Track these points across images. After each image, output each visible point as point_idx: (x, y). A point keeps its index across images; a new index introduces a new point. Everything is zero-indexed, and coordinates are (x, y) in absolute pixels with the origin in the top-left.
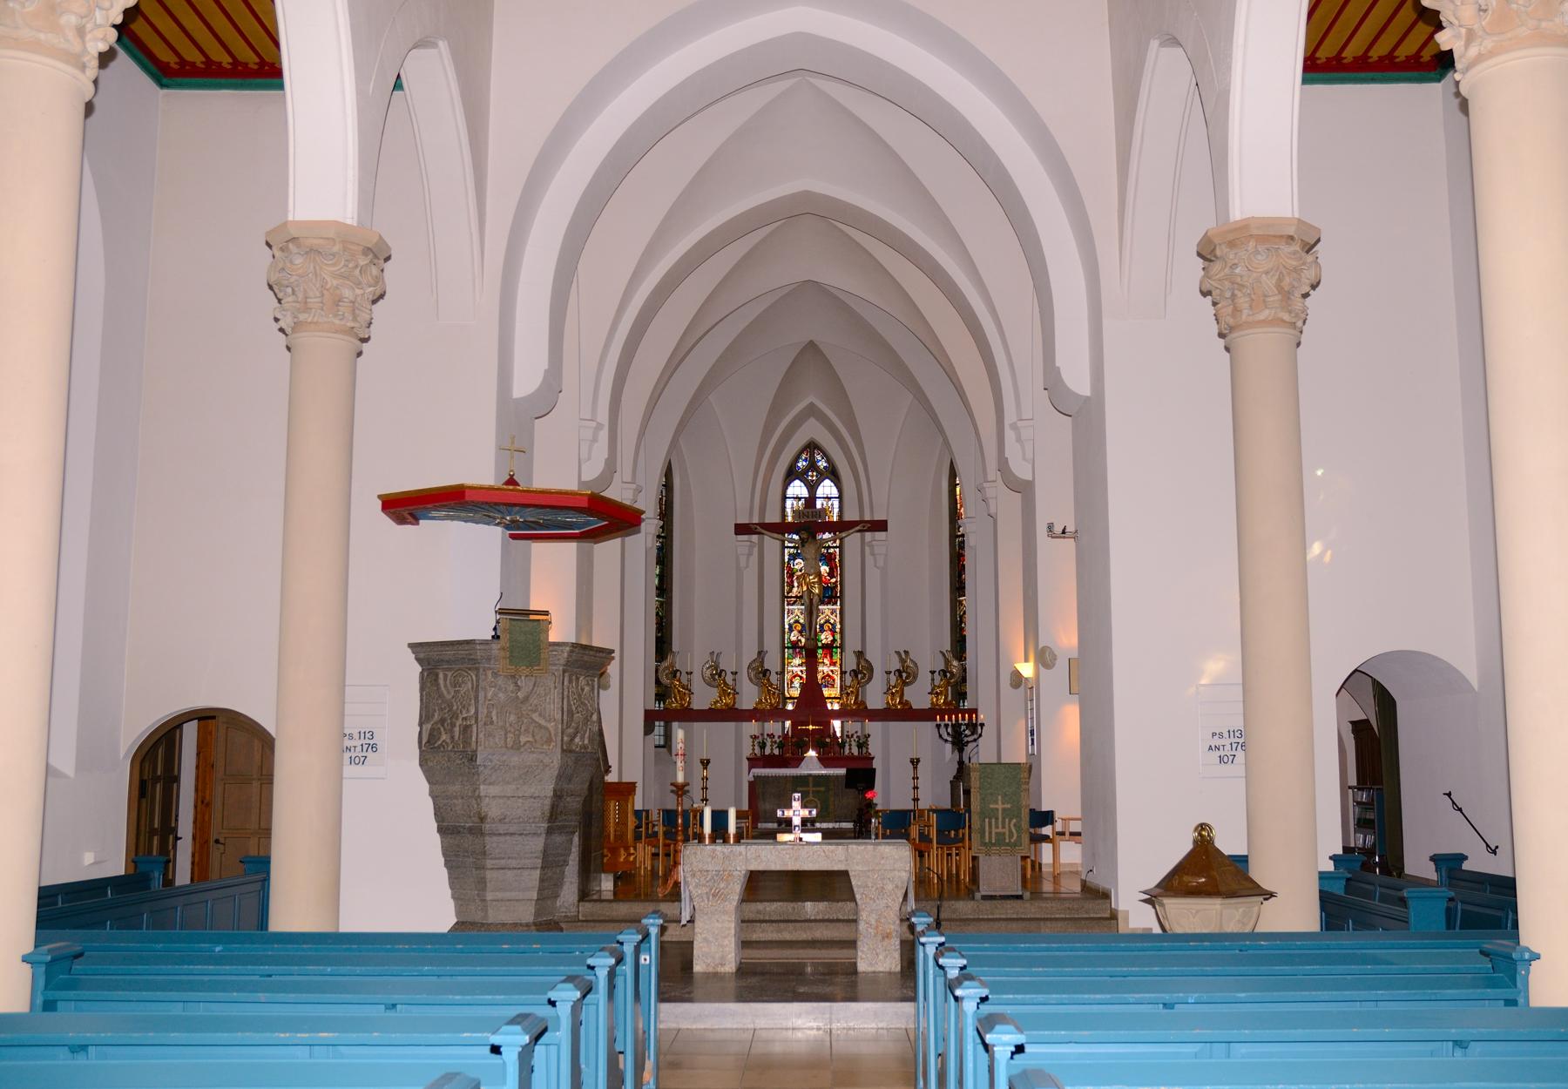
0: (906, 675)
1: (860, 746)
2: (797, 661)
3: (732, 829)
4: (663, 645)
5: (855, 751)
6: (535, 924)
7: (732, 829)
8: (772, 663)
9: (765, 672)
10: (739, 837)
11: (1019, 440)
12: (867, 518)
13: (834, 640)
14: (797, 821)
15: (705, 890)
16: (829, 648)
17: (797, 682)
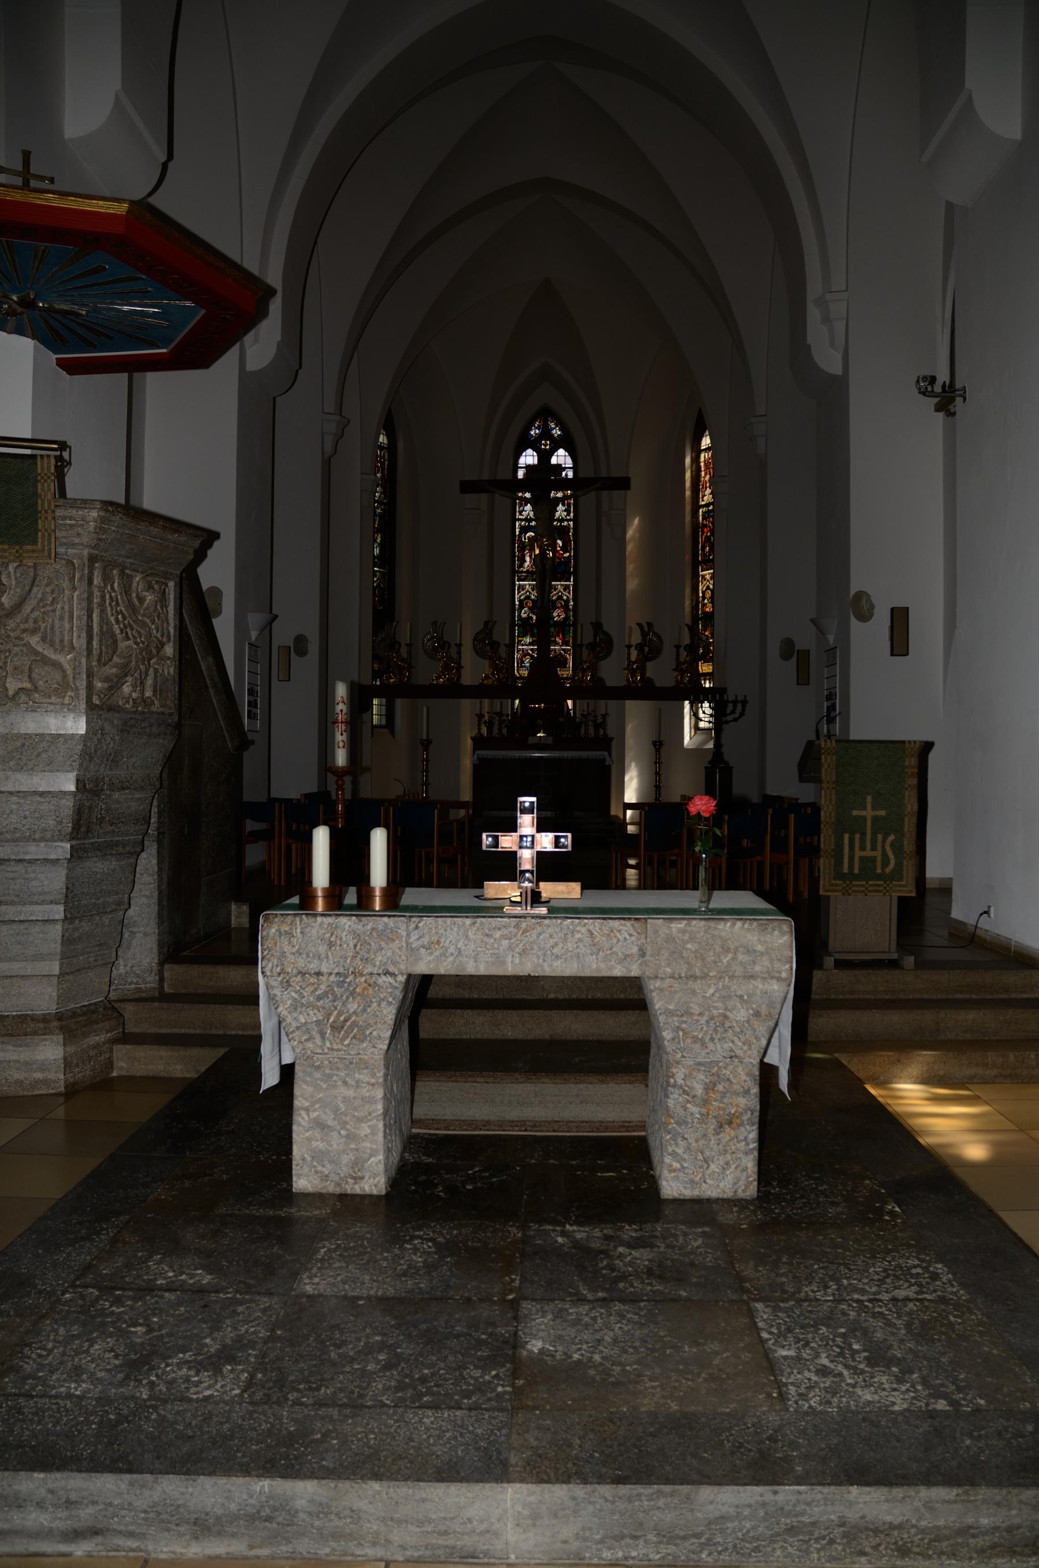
0: (650, 647)
1: (597, 727)
2: (532, 433)
3: (379, 875)
4: (384, 610)
5: (591, 731)
6: (59, 1017)
7: (379, 875)
8: (501, 634)
9: (495, 645)
10: (392, 901)
11: (826, 319)
12: (604, 474)
13: (567, 618)
14: (526, 858)
15: (314, 1016)
16: (562, 626)
17: (527, 662)
